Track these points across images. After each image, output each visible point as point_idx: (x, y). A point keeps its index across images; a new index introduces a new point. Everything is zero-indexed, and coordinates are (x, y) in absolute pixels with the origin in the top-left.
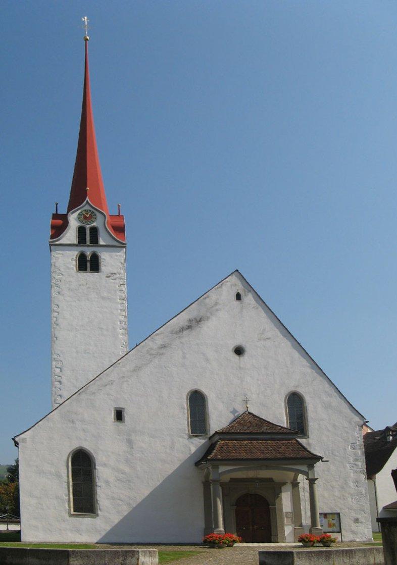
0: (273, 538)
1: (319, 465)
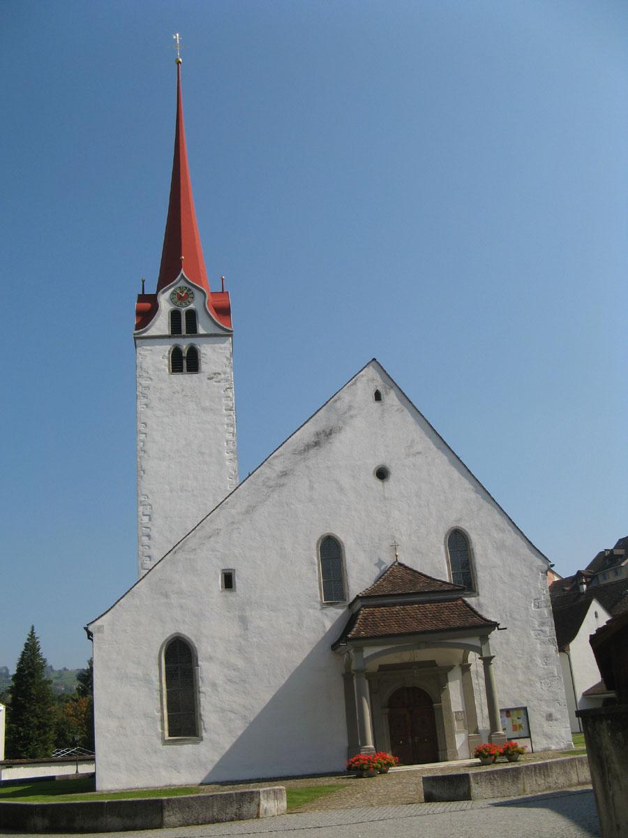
1: (495, 635)
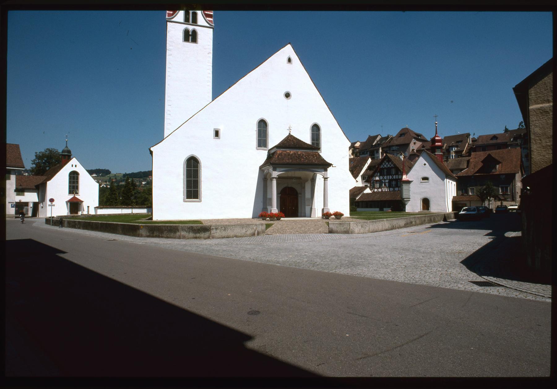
0: (299, 214)
1: (330, 169)
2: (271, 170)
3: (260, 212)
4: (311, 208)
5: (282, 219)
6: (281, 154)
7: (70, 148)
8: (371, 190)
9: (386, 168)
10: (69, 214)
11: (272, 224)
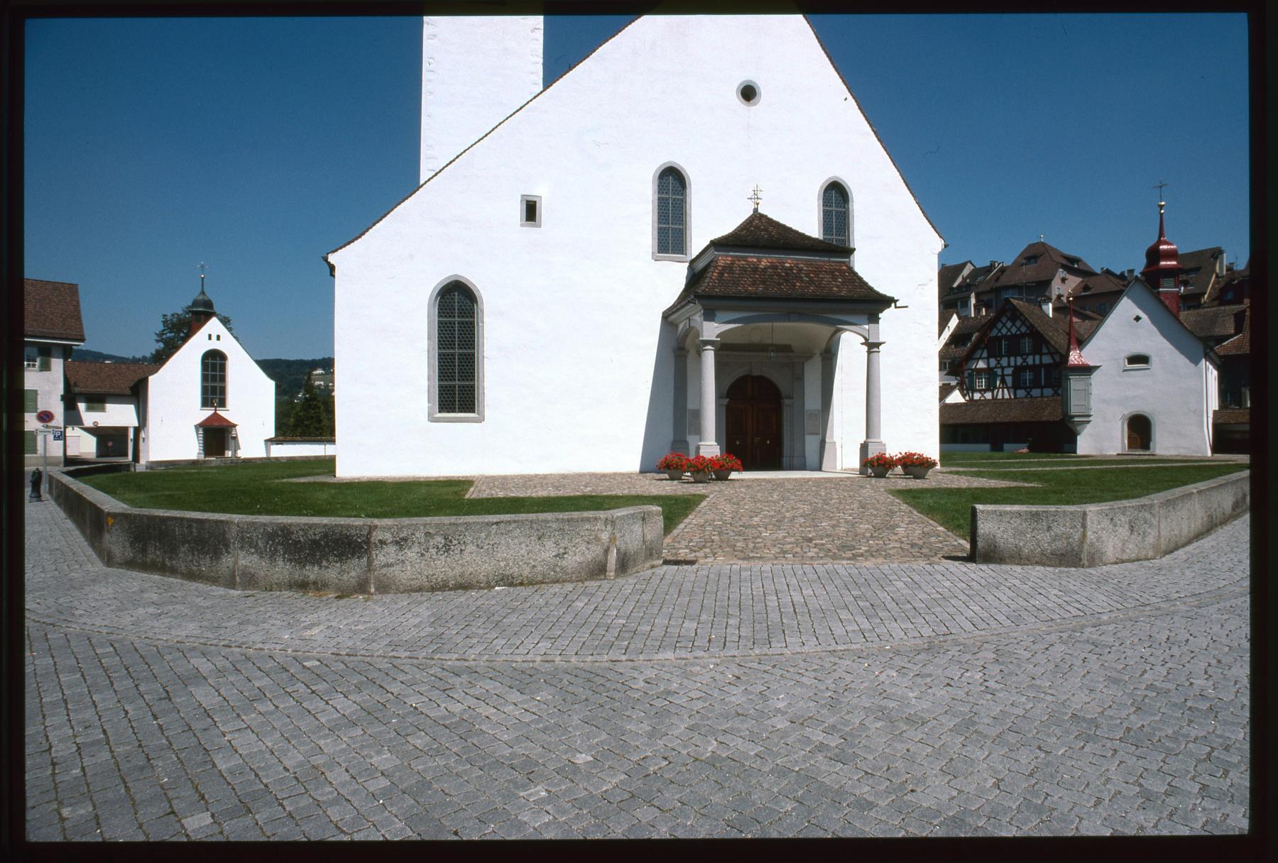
0: (785, 460)
1: (886, 315)
2: (698, 318)
3: (664, 452)
4: (823, 442)
5: (734, 475)
6: (729, 268)
7: (211, 295)
8: (964, 396)
9: (1005, 337)
10: (202, 457)
11: (703, 497)
